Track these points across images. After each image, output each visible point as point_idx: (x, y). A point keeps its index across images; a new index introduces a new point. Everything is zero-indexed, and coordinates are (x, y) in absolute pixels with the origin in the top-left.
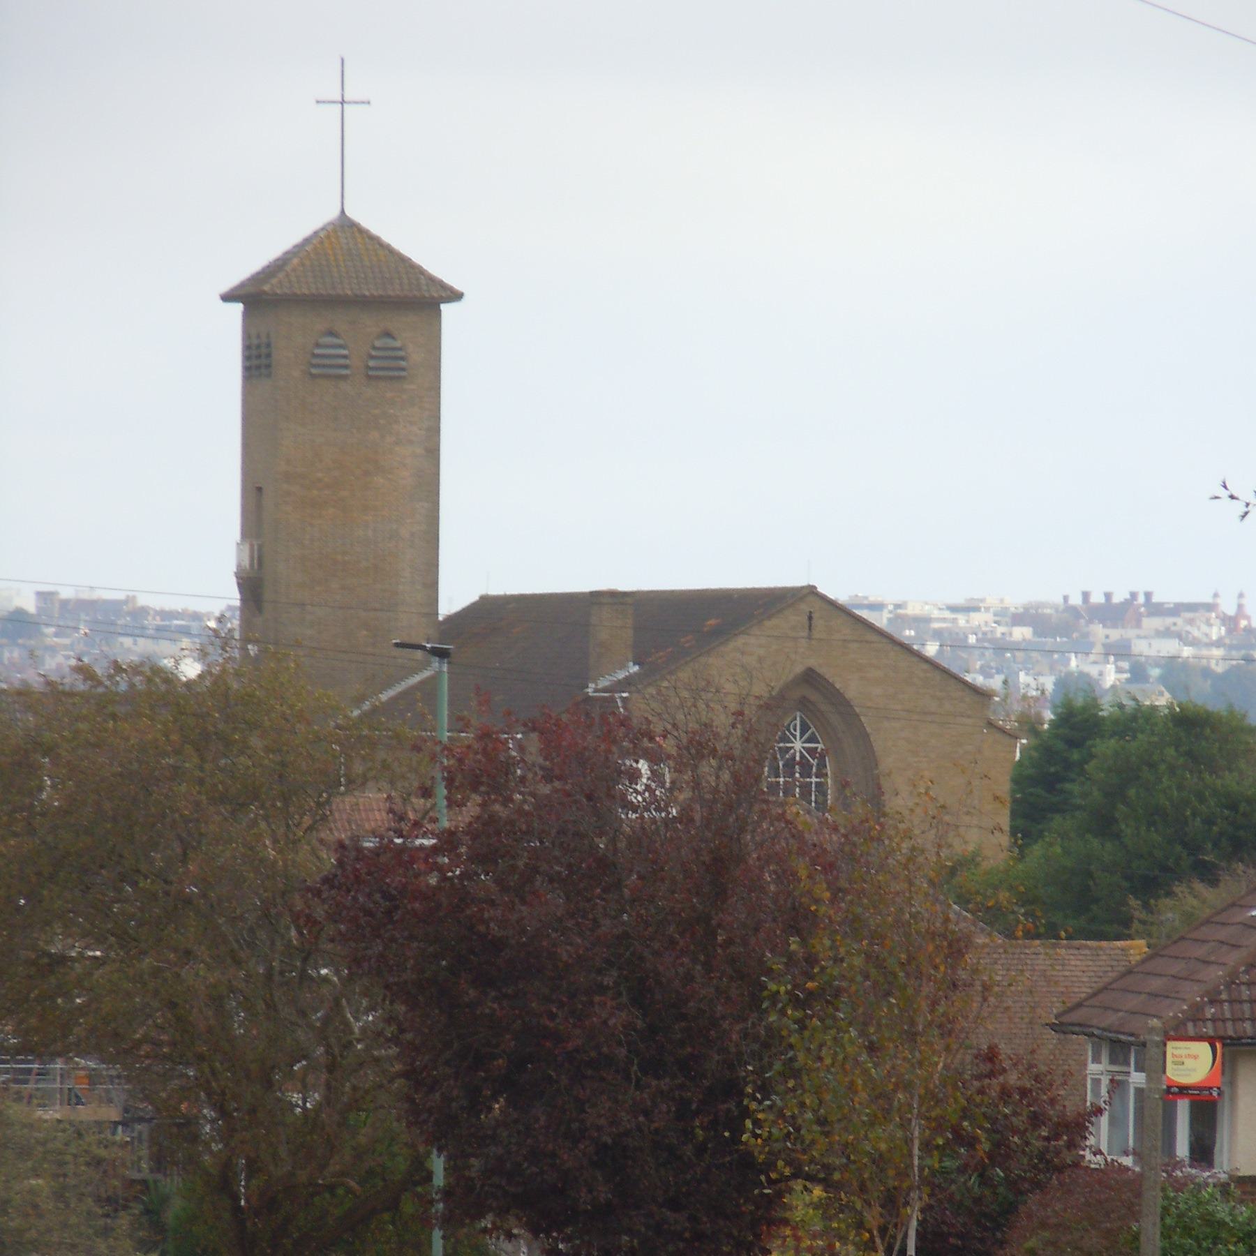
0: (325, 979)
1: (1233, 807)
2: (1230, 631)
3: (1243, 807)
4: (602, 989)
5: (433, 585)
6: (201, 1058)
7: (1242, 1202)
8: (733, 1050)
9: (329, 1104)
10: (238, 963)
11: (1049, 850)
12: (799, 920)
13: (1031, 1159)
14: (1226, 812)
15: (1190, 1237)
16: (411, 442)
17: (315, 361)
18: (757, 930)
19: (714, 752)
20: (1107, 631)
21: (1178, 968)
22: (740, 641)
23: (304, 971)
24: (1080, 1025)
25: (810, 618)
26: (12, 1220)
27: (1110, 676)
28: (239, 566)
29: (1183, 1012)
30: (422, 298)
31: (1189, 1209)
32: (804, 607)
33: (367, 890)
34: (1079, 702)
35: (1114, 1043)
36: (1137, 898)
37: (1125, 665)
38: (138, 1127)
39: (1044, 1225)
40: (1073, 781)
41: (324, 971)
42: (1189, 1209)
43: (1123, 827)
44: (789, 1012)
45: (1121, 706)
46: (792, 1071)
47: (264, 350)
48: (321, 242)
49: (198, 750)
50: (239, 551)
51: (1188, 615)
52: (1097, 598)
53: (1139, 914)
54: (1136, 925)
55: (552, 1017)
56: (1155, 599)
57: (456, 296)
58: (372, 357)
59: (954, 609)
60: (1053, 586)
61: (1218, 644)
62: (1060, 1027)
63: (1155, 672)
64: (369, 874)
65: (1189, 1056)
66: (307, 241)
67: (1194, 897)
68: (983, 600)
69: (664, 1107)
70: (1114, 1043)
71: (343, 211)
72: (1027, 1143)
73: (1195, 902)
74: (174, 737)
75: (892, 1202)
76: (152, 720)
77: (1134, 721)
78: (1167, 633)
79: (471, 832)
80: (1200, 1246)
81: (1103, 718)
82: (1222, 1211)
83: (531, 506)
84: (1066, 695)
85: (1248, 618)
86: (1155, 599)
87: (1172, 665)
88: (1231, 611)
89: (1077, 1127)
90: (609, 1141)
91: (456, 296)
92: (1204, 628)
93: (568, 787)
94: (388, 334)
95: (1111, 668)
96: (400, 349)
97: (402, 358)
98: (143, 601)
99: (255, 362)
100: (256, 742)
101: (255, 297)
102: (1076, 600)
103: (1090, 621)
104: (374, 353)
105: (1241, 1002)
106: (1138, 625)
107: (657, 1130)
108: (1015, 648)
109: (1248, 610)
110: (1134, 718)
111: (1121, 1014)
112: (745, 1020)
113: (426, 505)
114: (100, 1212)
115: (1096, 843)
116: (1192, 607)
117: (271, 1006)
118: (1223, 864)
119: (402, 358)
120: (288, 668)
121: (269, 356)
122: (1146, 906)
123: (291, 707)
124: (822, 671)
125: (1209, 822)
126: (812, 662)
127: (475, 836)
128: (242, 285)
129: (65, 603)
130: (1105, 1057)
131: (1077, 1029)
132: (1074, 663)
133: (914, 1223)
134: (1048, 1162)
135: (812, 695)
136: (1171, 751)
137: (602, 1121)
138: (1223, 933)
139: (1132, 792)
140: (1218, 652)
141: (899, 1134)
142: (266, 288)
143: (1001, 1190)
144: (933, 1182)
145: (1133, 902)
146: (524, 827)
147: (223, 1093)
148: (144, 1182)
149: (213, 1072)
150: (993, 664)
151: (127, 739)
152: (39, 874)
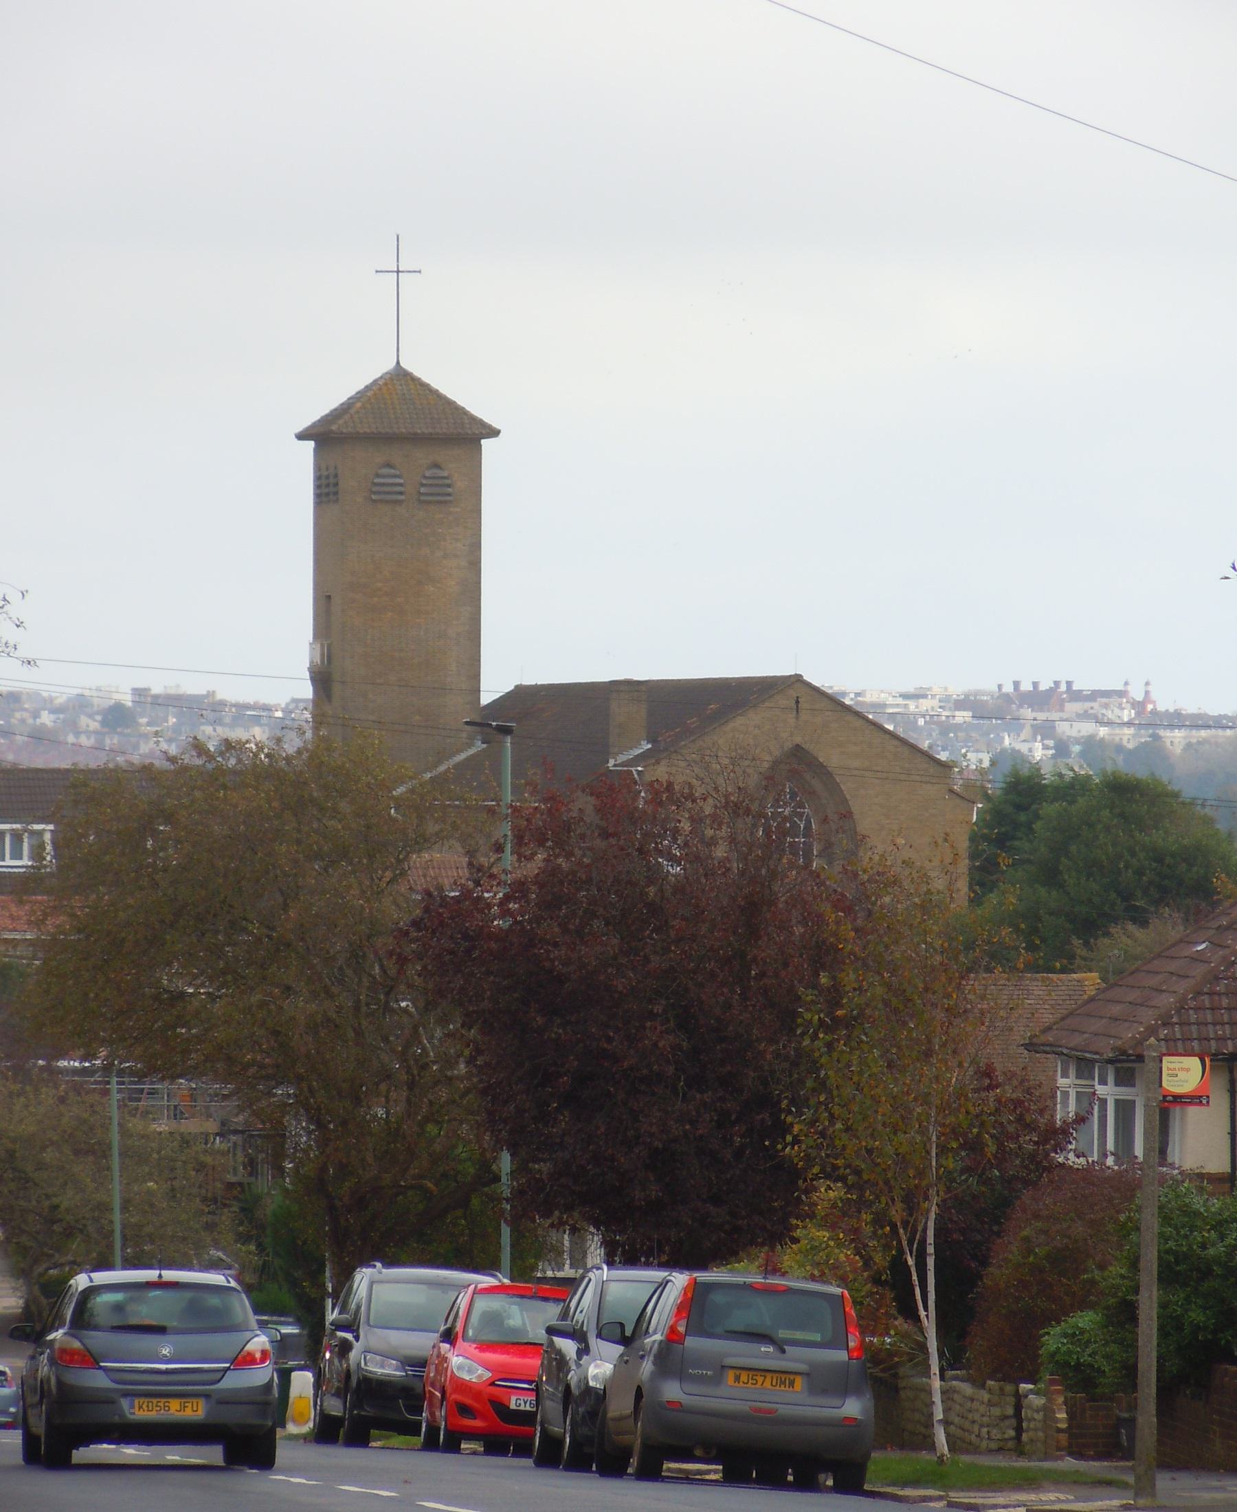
0: (405, 1010)
1: (1160, 860)
2: (1138, 714)
3: (1168, 860)
4: (652, 1016)
5: (476, 677)
6: (300, 1078)
7: (1212, 1194)
8: (766, 1068)
9: (409, 1116)
10: (331, 996)
11: (1009, 896)
12: (823, 955)
13: (1023, 1161)
14: (1154, 865)
15: (1170, 1225)
17: (375, 489)
18: (786, 965)
19: (748, 811)
20: (1035, 715)
21: (1133, 996)
22: (740, 721)
23: (387, 1002)
24: (1051, 1045)
25: (797, 702)
26: (133, 1216)
27: (1039, 752)
28: (311, 662)
29: (1140, 1033)
30: (463, 435)
31: (1169, 1202)
32: (793, 693)
33: (449, 933)
34: (1025, 772)
35: (1080, 1060)
36: (1079, 938)
37: (1051, 743)
38: (233, 1138)
39: (1037, 1216)
40: (1021, 839)
41: (403, 1004)
42: (1169, 1202)
43: (1066, 877)
44: (821, 1036)
45: (1061, 775)
46: (822, 1085)
47: (332, 480)
48: (380, 389)
49: (296, 815)
50: (312, 649)
51: (1104, 700)
52: (1026, 686)
53: (1081, 951)
54: (1078, 961)
55: (610, 1040)
56: (1075, 688)
57: (494, 433)
58: (423, 485)
59: (905, 696)
60: (988, 676)
61: (1129, 724)
62: (1031, 1046)
63: (1076, 749)
64: (452, 918)
65: (1183, 1069)
66: (367, 388)
67: (1125, 940)
68: (929, 689)
69: (707, 1117)
70: (1080, 1060)
71: (398, 362)
72: (1020, 1148)
73: (1129, 942)
74: (275, 804)
75: (911, 1202)
76: (257, 789)
77: (1071, 789)
78: (1085, 716)
79: (537, 880)
80: (1178, 1233)
81: (1045, 786)
82: (1197, 1203)
83: (557, 610)
84: (1014, 766)
85: (1154, 702)
86: (1075, 688)
87: (1090, 743)
88: (1139, 697)
89: (1058, 1136)
90: (660, 1146)
91: (494, 433)
92: (1117, 711)
93: (622, 842)
95: (1038, 745)
97: (449, 486)
98: (220, 696)
99: (325, 490)
100: (344, 806)
101: (326, 436)
102: (1008, 688)
103: (1021, 706)
104: (424, 482)
105: (1190, 1024)
106: (1062, 710)
107: (701, 1136)
108: (957, 728)
109: (1153, 696)
110: (1071, 785)
111: (1086, 1036)
112: (777, 1043)
114: (207, 1210)
115: (1042, 891)
116: (1107, 694)
117: (359, 1033)
118: (1152, 909)
120: (373, 744)
121: (336, 484)
122: (1086, 944)
123: (375, 778)
124: (806, 746)
125: (1140, 872)
126: (798, 740)
127: (541, 886)
128: (314, 425)
129: (156, 697)
130: (1072, 1072)
131: (1048, 1049)
132: (1007, 741)
133: (933, 1216)
134: (1039, 1163)
135: (799, 766)
136: (1106, 813)
137: (654, 1129)
138: (1173, 966)
139: (1073, 848)
140: (1129, 731)
141: (918, 1139)
142: (334, 428)
143: (998, 1187)
144: (948, 1178)
145: (1076, 942)
146: (584, 877)
147: (319, 1109)
148: (240, 1184)
149: (311, 1090)
150: (939, 743)
151: (236, 806)
152: (162, 922)
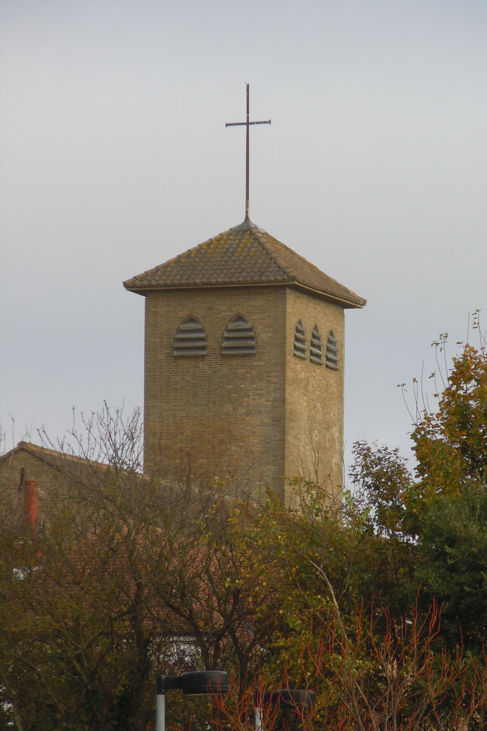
16: (259, 412)
71: (247, 219)
94: (240, 318)
96: (250, 330)
97: (252, 338)
113: (272, 468)
119: (252, 338)
